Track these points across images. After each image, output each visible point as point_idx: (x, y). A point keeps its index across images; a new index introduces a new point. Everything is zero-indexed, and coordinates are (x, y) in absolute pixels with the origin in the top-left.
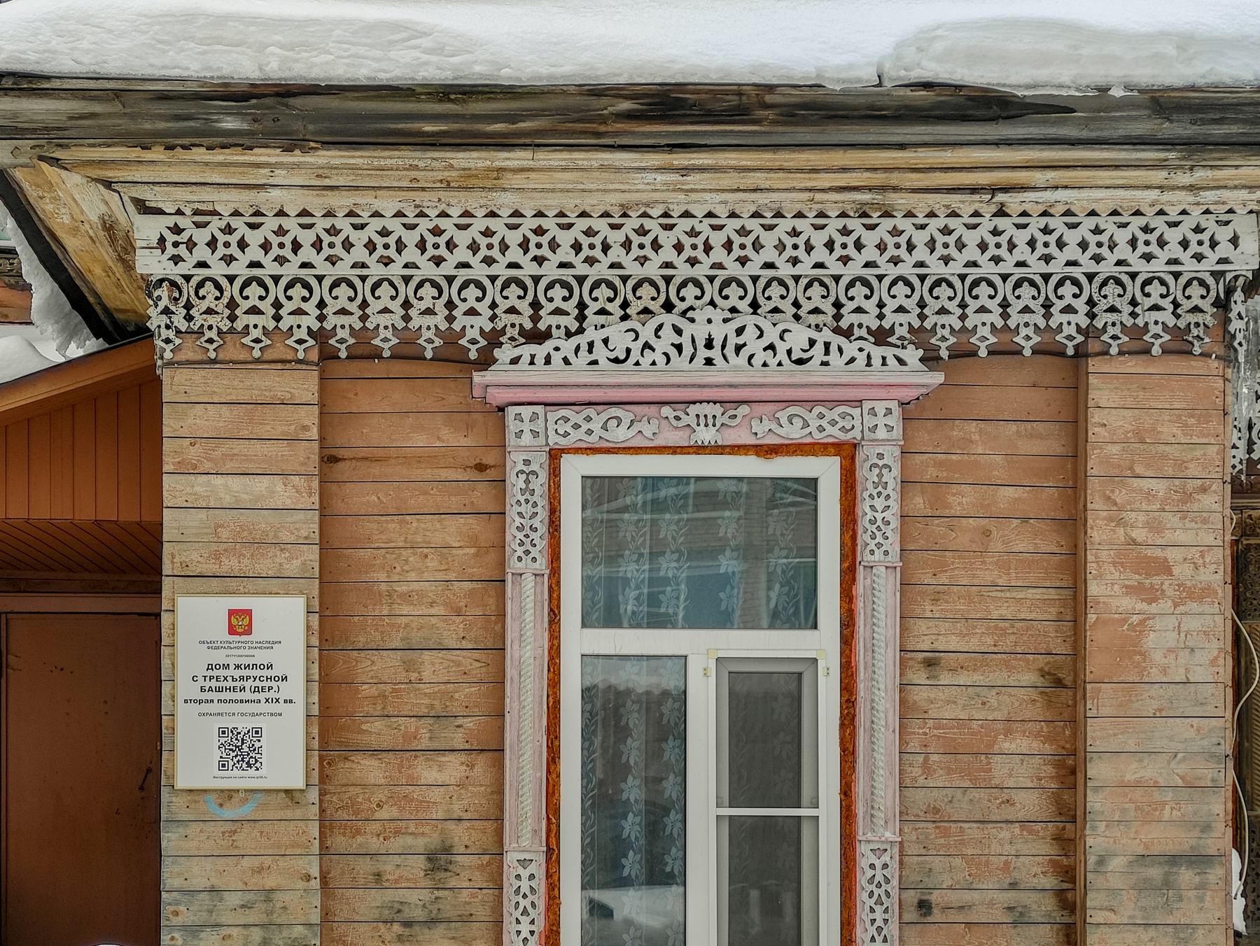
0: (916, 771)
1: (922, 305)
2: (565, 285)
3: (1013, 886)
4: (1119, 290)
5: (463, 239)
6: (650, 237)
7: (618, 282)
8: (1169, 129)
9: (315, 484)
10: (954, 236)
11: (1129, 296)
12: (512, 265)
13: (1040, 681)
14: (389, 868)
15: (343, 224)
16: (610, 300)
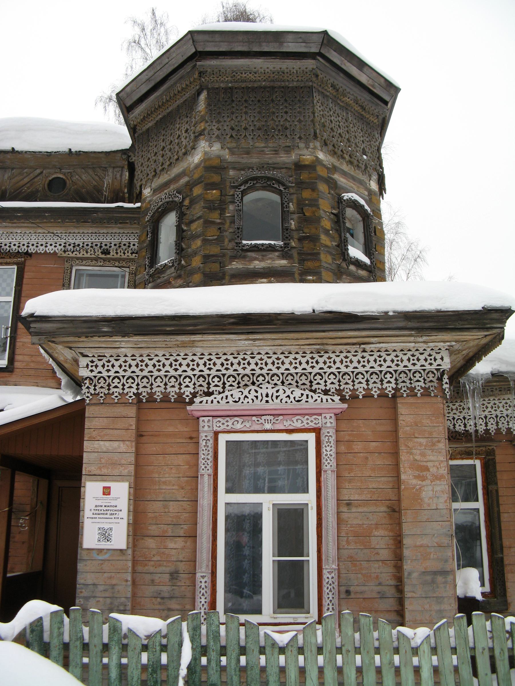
0: (344, 543)
1: (339, 381)
2: (218, 377)
3: (380, 584)
4: (405, 375)
5: (184, 363)
6: (247, 361)
7: (236, 376)
8: (410, 324)
9: (134, 444)
10: (349, 359)
11: (409, 377)
12: (201, 371)
13: (387, 510)
14: (157, 578)
15: (146, 359)
16: (234, 382)
